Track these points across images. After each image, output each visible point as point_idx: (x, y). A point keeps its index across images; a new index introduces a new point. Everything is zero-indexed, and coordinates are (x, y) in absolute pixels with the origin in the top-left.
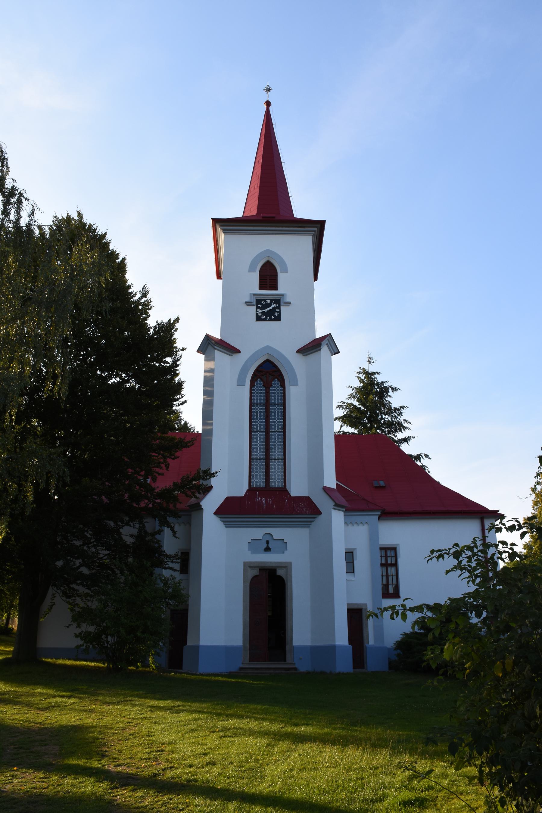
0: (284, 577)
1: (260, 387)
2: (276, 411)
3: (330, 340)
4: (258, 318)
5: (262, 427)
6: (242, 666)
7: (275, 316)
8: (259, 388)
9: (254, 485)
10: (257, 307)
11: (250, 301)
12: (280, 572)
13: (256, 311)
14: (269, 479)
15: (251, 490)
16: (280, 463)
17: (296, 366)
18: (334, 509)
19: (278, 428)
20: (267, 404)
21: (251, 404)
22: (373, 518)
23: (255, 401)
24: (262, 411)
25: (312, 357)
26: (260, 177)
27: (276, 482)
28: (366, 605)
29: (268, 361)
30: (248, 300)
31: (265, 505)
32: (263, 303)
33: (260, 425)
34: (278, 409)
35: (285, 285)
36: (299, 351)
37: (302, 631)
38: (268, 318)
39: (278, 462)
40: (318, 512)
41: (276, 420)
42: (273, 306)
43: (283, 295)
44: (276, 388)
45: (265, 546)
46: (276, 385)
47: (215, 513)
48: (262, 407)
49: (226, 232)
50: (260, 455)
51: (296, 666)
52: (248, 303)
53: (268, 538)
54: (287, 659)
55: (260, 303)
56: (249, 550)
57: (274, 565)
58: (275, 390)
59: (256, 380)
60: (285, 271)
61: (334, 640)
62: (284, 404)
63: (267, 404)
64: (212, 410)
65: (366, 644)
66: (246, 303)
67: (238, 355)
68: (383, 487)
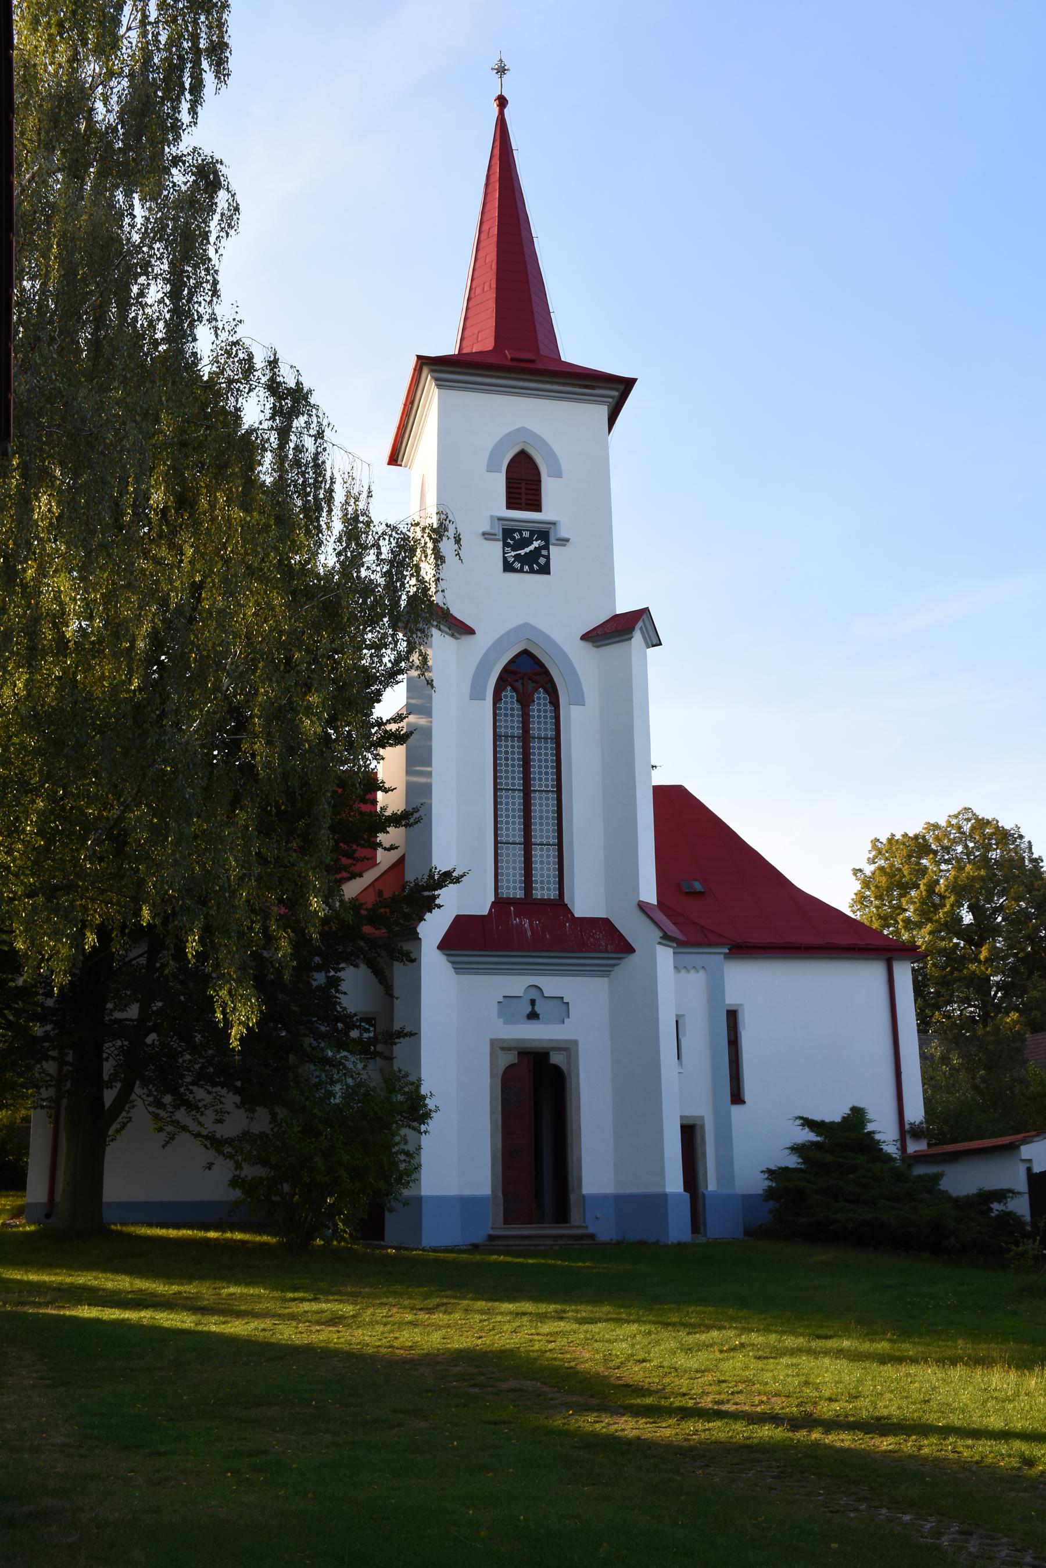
0: (564, 1068)
1: (512, 703)
2: (543, 751)
3: (647, 622)
4: (508, 567)
5: (517, 781)
6: (491, 1232)
7: (538, 564)
8: (509, 706)
9: (504, 893)
10: (506, 545)
11: (493, 531)
12: (556, 1059)
13: (504, 553)
14: (531, 882)
15: (500, 903)
16: (551, 853)
17: (580, 666)
18: (660, 943)
19: (547, 786)
20: (526, 738)
21: (496, 737)
22: (713, 958)
23: (503, 731)
24: (516, 750)
25: (614, 651)
26: (494, 267)
27: (544, 891)
28: (702, 1118)
29: (526, 653)
30: (487, 528)
31: (529, 933)
32: (517, 536)
33: (513, 778)
34: (546, 748)
35: (556, 503)
36: (585, 637)
37: (598, 1169)
38: (526, 568)
39: (548, 850)
40: (625, 948)
41: (543, 770)
42: (536, 544)
43: (554, 524)
44: (542, 708)
45: (529, 1009)
46: (542, 701)
47: (439, 947)
48: (516, 744)
49: (440, 384)
50: (514, 836)
51: (591, 1230)
52: (487, 536)
53: (534, 994)
54: (572, 1218)
55: (510, 536)
56: (500, 1016)
57: (545, 1045)
58: (539, 711)
59: (504, 689)
60: (557, 474)
61: (664, 1186)
62: (557, 739)
63: (526, 738)
64: (431, 746)
65: (702, 1189)
66: (484, 534)
67: (470, 638)
68: (701, 893)
